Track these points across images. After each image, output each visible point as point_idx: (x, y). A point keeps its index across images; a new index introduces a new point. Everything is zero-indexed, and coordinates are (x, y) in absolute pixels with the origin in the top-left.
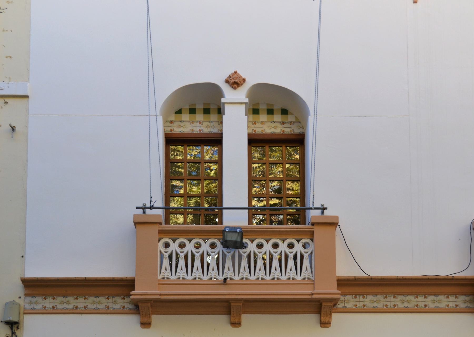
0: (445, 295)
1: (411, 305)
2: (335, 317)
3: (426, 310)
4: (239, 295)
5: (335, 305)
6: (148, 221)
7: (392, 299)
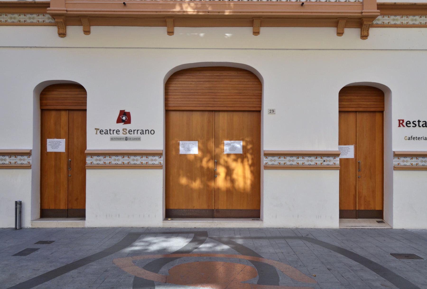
1: (16, 21)
2: (373, 31)
4: (114, 11)
7: (5, 16)
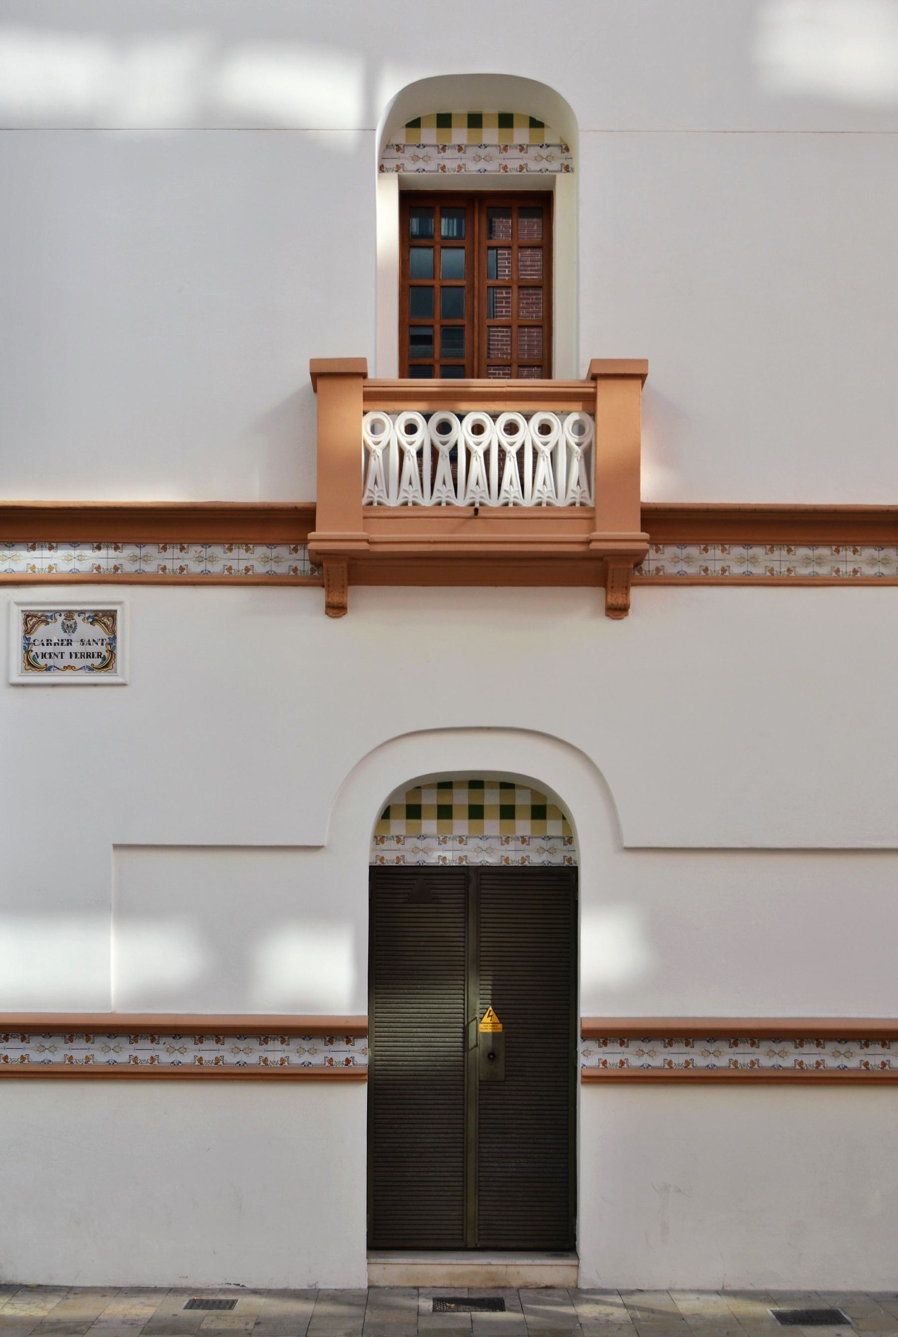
0: (831, 546)
2: (638, 596)
3: (856, 581)
5: (638, 565)
6: (333, 371)
